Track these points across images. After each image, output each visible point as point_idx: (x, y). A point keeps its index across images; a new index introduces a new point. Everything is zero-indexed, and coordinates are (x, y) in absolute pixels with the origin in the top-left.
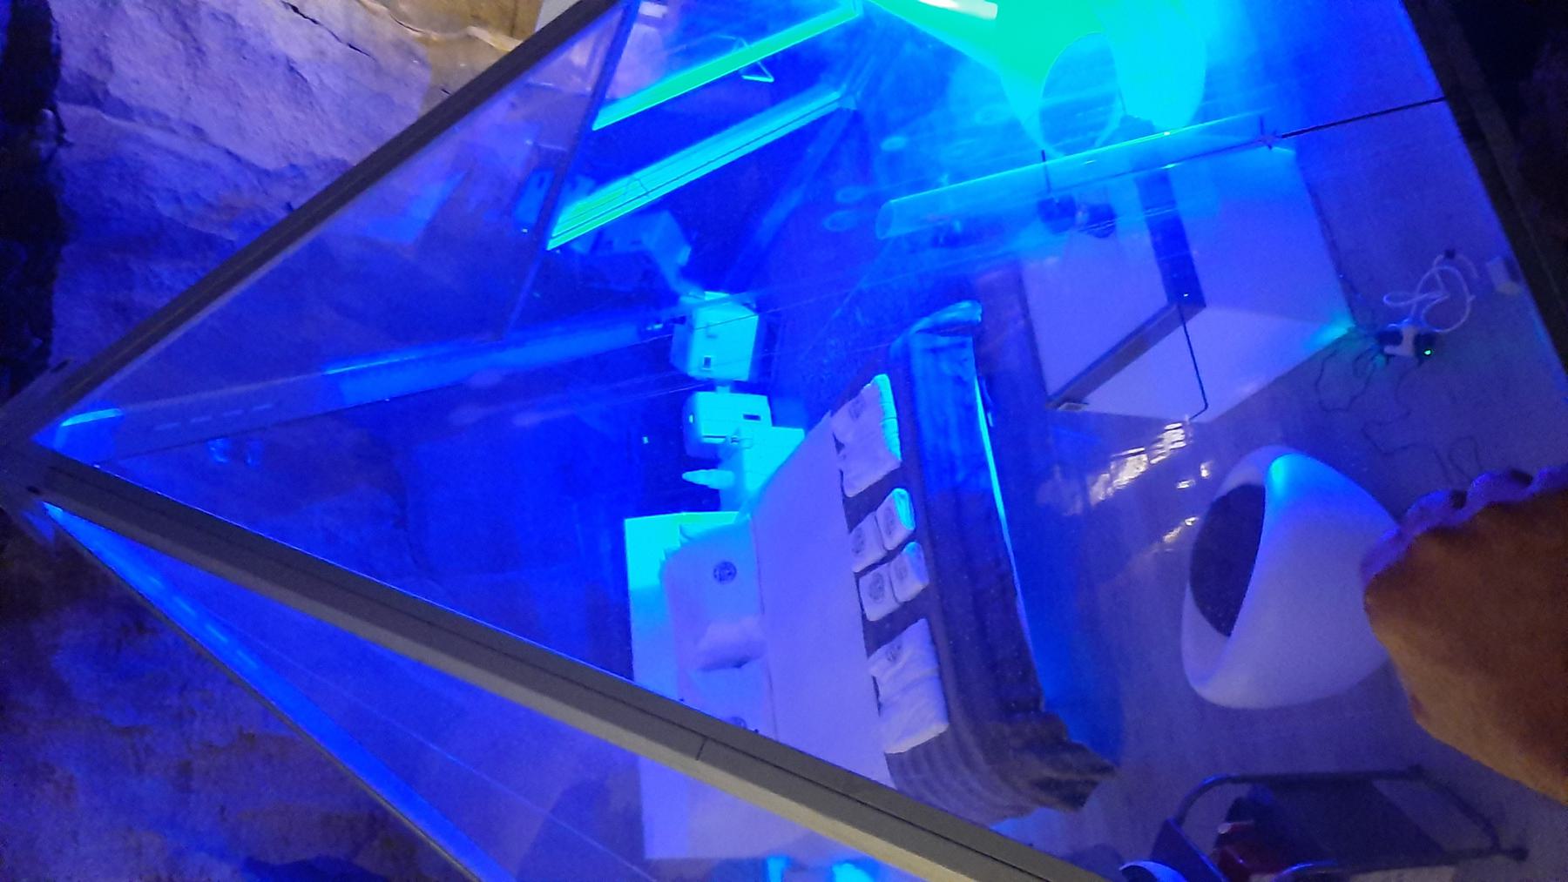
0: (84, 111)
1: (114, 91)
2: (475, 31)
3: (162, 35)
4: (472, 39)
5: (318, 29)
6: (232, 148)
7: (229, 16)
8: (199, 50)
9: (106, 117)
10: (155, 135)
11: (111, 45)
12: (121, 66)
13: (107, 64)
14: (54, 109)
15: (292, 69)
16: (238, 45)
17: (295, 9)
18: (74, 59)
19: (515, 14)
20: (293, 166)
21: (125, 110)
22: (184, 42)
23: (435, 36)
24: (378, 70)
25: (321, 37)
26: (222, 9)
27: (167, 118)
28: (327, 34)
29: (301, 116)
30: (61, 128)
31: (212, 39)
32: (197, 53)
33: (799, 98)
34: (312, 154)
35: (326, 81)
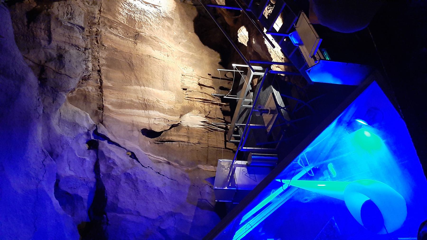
0: (113, 214)
1: (119, 206)
2: (200, 166)
3: (129, 189)
4: (199, 168)
5: (164, 177)
6: (146, 216)
7: (144, 181)
8: (138, 191)
9: (118, 215)
10: (128, 217)
11: (118, 194)
12: (121, 199)
13: (117, 199)
14: (106, 215)
15: (159, 190)
16: (147, 187)
17: (159, 173)
18: (110, 198)
19: (207, 156)
20: (160, 216)
21: (121, 211)
22: (134, 190)
23: (190, 169)
24: (178, 184)
25: (165, 179)
26: (143, 179)
27: (131, 210)
28: (166, 178)
29: (161, 202)
30: (108, 220)
31: (141, 186)
32: (137, 190)
33: (326, 196)
34: (164, 212)
35: (166, 191)
